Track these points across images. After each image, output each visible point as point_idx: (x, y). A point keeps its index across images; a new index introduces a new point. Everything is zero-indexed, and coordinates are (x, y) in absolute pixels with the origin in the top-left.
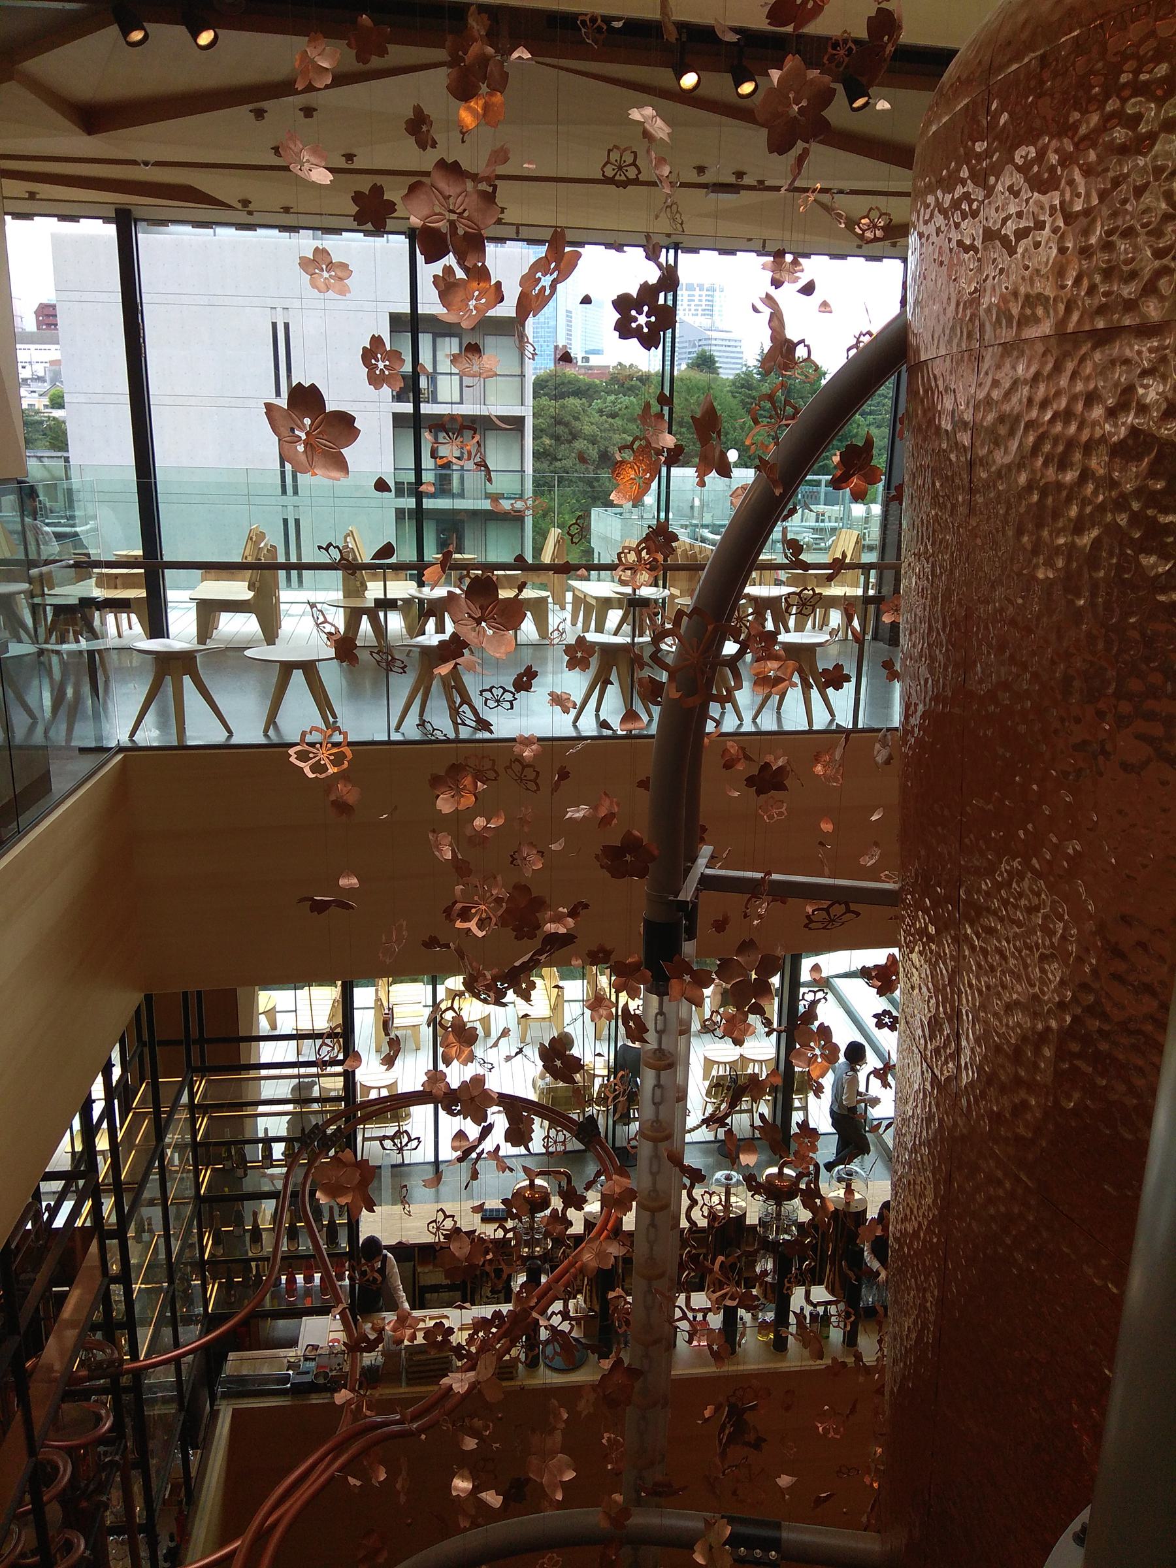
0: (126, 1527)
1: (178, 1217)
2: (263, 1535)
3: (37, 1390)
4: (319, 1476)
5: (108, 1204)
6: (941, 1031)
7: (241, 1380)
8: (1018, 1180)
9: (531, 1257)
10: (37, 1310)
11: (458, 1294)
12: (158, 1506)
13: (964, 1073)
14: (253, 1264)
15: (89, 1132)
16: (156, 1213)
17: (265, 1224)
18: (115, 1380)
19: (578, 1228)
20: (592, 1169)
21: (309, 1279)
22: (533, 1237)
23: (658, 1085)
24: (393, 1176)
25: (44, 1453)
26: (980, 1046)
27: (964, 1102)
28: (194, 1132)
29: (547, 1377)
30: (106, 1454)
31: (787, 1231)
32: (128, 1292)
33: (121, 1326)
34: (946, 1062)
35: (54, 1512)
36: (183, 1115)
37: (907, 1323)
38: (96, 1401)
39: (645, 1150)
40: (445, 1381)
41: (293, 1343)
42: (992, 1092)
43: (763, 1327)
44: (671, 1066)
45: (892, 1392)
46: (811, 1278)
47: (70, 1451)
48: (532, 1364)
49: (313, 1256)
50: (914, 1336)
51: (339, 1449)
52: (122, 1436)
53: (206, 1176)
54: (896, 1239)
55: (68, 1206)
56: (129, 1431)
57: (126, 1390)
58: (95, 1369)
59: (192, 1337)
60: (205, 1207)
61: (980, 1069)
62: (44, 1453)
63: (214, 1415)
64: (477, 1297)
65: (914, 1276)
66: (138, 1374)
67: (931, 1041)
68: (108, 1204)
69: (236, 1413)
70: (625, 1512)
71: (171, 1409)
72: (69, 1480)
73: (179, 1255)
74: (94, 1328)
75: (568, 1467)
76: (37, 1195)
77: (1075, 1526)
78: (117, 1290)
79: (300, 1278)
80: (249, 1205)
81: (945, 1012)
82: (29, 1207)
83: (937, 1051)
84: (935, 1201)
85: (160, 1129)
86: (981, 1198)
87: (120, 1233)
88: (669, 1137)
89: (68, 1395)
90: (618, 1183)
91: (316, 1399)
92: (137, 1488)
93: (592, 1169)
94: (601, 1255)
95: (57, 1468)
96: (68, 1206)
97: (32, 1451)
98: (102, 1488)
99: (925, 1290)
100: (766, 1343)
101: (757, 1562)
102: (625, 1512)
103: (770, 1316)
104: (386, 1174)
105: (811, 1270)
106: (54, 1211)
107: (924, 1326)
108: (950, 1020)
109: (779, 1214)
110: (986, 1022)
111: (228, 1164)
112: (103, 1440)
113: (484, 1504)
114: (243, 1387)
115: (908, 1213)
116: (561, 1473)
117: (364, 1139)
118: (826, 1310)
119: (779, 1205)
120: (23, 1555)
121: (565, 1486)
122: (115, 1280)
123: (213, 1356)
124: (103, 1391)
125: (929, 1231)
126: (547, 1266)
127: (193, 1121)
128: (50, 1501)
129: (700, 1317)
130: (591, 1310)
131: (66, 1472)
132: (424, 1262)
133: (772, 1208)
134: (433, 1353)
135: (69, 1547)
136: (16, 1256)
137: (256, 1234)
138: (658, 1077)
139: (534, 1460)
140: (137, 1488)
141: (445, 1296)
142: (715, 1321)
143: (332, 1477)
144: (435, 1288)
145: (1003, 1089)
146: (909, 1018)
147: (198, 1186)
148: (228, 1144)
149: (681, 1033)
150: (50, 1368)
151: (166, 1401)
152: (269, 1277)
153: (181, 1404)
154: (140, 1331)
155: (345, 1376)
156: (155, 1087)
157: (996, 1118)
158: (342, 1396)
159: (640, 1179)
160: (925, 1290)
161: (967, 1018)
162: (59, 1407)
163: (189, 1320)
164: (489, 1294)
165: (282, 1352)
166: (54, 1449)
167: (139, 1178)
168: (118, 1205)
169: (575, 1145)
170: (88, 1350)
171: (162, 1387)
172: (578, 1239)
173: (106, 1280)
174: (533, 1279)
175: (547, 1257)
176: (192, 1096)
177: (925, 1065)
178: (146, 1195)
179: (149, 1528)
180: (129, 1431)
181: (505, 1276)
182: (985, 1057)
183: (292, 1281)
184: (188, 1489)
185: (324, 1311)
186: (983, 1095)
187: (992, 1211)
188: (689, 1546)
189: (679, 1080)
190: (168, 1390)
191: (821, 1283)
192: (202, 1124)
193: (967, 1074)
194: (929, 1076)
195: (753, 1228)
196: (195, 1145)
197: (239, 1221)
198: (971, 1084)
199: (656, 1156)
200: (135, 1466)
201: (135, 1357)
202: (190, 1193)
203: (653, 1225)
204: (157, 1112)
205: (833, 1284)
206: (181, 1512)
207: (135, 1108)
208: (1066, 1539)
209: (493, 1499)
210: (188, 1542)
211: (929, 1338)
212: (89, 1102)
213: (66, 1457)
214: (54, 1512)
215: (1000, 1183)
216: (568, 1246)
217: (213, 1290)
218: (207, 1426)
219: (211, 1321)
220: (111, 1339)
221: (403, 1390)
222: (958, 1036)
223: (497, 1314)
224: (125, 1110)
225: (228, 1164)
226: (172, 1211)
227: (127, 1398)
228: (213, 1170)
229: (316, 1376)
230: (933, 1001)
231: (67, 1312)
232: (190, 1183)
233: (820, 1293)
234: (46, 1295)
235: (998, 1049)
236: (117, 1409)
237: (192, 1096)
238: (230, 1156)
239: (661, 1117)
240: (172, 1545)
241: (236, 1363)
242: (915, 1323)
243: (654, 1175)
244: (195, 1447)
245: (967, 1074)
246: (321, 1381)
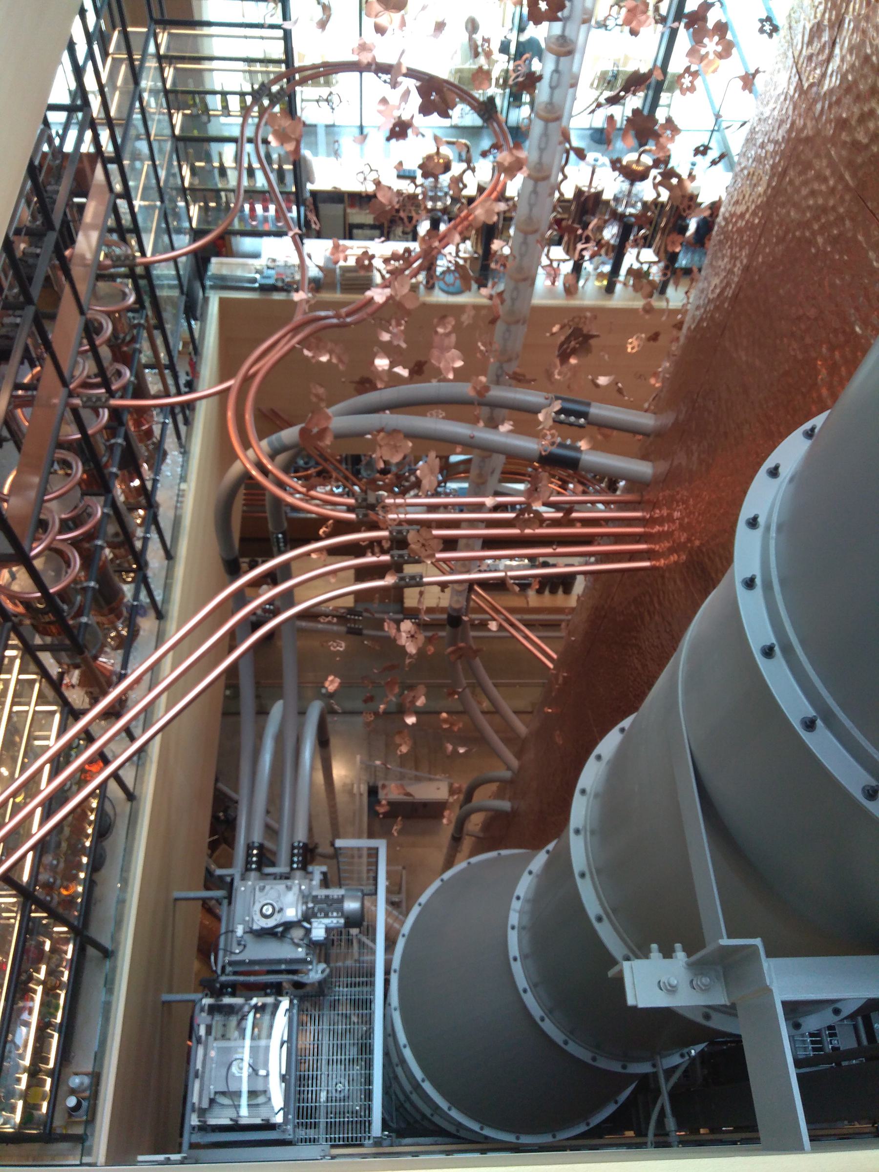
0: (155, 365)
1: (161, 150)
2: (248, 380)
3: (77, 271)
4: (282, 348)
5: (104, 135)
6: (820, 37)
7: (223, 278)
8: (841, 178)
9: (433, 210)
10: (65, 214)
11: (377, 232)
12: (175, 354)
13: (828, 79)
14: (223, 194)
15: (78, 72)
16: (143, 146)
17: (229, 162)
18: (132, 269)
19: (471, 191)
20: (486, 143)
21: (266, 209)
22: (436, 194)
23: (556, 71)
24: (328, 134)
25: (90, 315)
26: (851, 54)
27: (819, 106)
28: (164, 81)
29: (439, 297)
30: (134, 318)
31: (633, 206)
32: (131, 207)
33: (130, 231)
34: (815, 68)
35: (105, 352)
36: (152, 64)
37: (716, 281)
38: (121, 283)
39: (537, 128)
40: (369, 294)
41: (256, 256)
42: (847, 100)
43: (601, 276)
44: (570, 53)
45: (689, 328)
46: (647, 242)
47: (109, 314)
48: (430, 287)
49: (268, 192)
50: (718, 291)
51: (296, 330)
52: (143, 307)
53: (178, 119)
54: (725, 219)
55: (73, 134)
56: (147, 304)
57: (142, 277)
58: (117, 261)
59: (184, 244)
60: (181, 145)
61: (844, 77)
62: (90, 315)
63: (206, 300)
64: (392, 236)
65: (731, 247)
66: (147, 267)
67: (807, 47)
68: (104, 135)
69: (222, 301)
70: (486, 388)
71: (176, 293)
72: (210, 958)
73: (166, 180)
74: (111, 231)
75: (459, 358)
76: (46, 123)
77: (807, 426)
78: (122, 204)
79: (259, 208)
80: (214, 147)
81: (830, 20)
82: (42, 132)
83: (810, 58)
84: (765, 192)
85: (135, 75)
86: (804, 191)
87: (118, 159)
88: (558, 119)
89: (100, 277)
90: (504, 157)
91: (278, 296)
92: (159, 341)
93: (486, 143)
94: (489, 212)
95: (101, 324)
96: (73, 134)
97: (82, 312)
98: (134, 340)
99: (736, 258)
100: (600, 288)
101: (571, 424)
102: (486, 388)
103: (607, 268)
104: (321, 132)
105: (645, 237)
106: (63, 138)
107: (728, 284)
108: (831, 27)
109: (630, 192)
110: (864, 32)
111: (195, 111)
112: (129, 309)
113: (398, 375)
114: (223, 283)
115: (741, 198)
116: (453, 361)
117: (303, 100)
118: (649, 267)
119: (632, 184)
120: (89, 377)
121: (456, 371)
122: (119, 196)
123: (201, 259)
124: (126, 276)
125: (754, 214)
126: (446, 218)
127: (162, 70)
128: (101, 345)
129: (555, 264)
130: (476, 252)
131: (108, 329)
132: (352, 205)
133: (626, 186)
134: (362, 273)
135: (119, 374)
136: (40, 171)
137: (223, 171)
138: (557, 63)
139: (435, 352)
140: (159, 341)
141: (368, 232)
142: (567, 268)
143: (293, 348)
144: (361, 226)
145: (858, 98)
146: (793, 23)
147: (173, 127)
148: (193, 93)
149: (585, 21)
150: (83, 257)
151: (170, 287)
152: (236, 204)
153: (182, 292)
154: (144, 237)
155: (297, 283)
156: (125, 35)
157: (842, 124)
158: (298, 296)
159: (528, 152)
160: (736, 258)
161: (848, 25)
162: (95, 285)
163: (179, 231)
164: (400, 234)
165: (250, 261)
166: (97, 311)
167: (125, 116)
168: (113, 137)
169: (477, 121)
170: (109, 246)
171: (167, 277)
172: (471, 200)
173: (113, 196)
174: (435, 225)
175: (445, 210)
176: (157, 46)
177: (794, 70)
178: (132, 132)
179: (172, 367)
180: (147, 304)
181: (414, 221)
182: (853, 66)
183: (253, 209)
184: (194, 347)
185: (279, 234)
186: (838, 102)
187: (811, 202)
188: (537, 412)
189: (575, 69)
190: (171, 280)
191: (650, 246)
192: (169, 73)
193: (831, 80)
194: (795, 80)
195: (607, 202)
196: (166, 92)
197: (208, 158)
198: (831, 91)
199: (545, 134)
200: (156, 328)
201: (143, 254)
202: (168, 131)
203: (535, 192)
204: (131, 60)
205: (659, 248)
206: (191, 359)
207: (113, 54)
208: (798, 434)
209: (404, 372)
210: (198, 377)
211: (729, 293)
212: (71, 47)
213: (107, 317)
214: (105, 352)
215: (825, 180)
216: (462, 203)
217: (194, 211)
218: (202, 308)
219: (196, 234)
220: (124, 239)
221: (338, 296)
222: (834, 43)
223: (407, 250)
224: (105, 54)
225: (195, 111)
226: (155, 146)
227: (142, 283)
228: (184, 115)
229: (277, 280)
230: (822, 7)
231: (89, 215)
232: (166, 124)
233: (648, 255)
234: (69, 204)
235: (867, 59)
236: (137, 288)
237: (157, 46)
238: (195, 105)
239: (554, 100)
240: (189, 378)
241: (217, 265)
242: (721, 282)
243: (541, 150)
244: (196, 319)
245: (831, 80)
246: (280, 284)
